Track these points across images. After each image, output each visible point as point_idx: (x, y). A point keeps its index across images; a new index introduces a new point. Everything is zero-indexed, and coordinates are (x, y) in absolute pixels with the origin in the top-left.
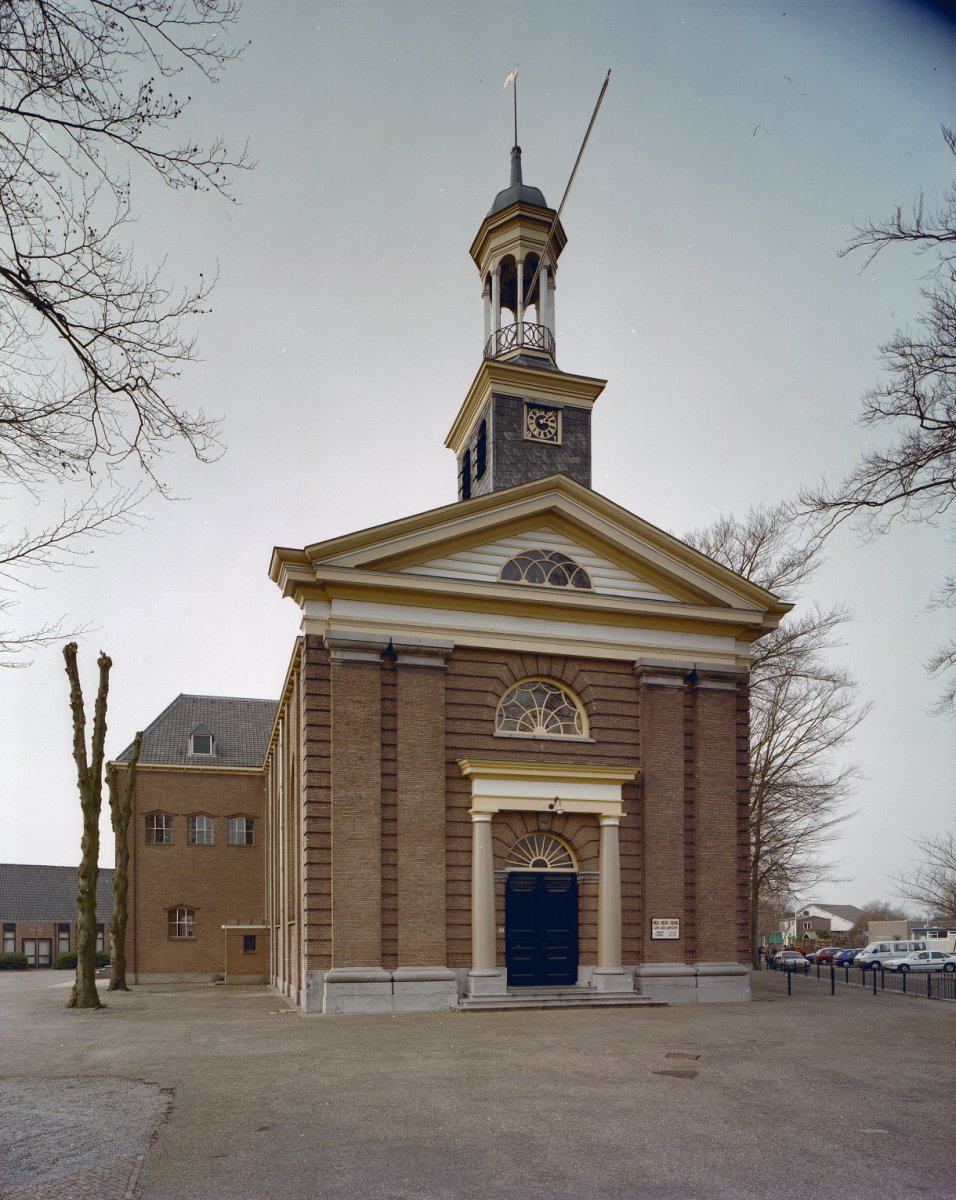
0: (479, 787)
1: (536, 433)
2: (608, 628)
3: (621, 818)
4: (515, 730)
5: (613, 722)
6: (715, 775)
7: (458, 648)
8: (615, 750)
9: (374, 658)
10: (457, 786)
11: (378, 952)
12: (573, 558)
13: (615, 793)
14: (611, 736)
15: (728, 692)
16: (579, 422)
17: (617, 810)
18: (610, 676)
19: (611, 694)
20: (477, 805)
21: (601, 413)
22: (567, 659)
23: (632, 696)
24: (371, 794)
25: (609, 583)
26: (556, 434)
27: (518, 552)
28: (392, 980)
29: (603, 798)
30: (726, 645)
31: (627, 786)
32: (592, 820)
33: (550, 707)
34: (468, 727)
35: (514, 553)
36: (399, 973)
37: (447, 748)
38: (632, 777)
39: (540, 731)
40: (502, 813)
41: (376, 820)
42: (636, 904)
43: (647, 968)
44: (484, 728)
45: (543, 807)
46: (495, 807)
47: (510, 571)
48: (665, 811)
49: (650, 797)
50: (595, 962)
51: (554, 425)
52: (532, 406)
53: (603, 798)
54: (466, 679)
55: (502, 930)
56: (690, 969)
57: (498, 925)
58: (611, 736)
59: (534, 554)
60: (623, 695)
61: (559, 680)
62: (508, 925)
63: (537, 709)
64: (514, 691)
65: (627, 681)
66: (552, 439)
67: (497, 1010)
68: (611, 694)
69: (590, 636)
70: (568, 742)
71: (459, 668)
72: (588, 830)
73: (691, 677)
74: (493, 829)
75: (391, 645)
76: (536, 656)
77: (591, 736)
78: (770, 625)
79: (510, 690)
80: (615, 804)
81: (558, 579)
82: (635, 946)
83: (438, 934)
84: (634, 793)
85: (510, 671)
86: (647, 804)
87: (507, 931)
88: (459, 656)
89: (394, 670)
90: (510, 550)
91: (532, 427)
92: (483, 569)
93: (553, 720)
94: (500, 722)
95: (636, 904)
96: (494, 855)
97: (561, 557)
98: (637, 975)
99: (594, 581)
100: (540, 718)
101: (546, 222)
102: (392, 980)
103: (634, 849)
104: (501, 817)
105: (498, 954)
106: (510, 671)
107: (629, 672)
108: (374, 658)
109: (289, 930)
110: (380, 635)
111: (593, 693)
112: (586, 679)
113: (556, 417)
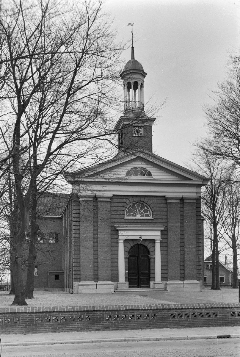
0: (120, 233)
2: (159, 187)
3: (161, 240)
4: (131, 216)
5: (159, 213)
6: (189, 227)
8: (160, 221)
9: (178, 201)
10: (115, 232)
11: (93, 277)
12: (147, 168)
13: (159, 233)
14: (158, 217)
15: (194, 203)
16: (149, 130)
17: (159, 238)
18: (158, 200)
19: (158, 205)
20: (120, 238)
21: (155, 127)
22: (145, 196)
23: (165, 205)
24: (91, 235)
25: (157, 175)
26: (142, 133)
27: (130, 168)
28: (97, 285)
29: (155, 234)
30: (194, 190)
31: (162, 231)
32: (153, 241)
33: (141, 209)
35: (129, 168)
38: (163, 229)
39: (138, 216)
40: (126, 239)
41: (92, 242)
42: (166, 264)
43: (169, 282)
44: (121, 216)
45: (138, 238)
46: (124, 238)
47: (128, 173)
48: (174, 237)
49: (170, 234)
50: (154, 280)
51: (141, 131)
53: (155, 234)
54: (117, 203)
55: (127, 271)
56: (182, 282)
58: (158, 217)
59: (136, 168)
60: (162, 205)
61: (143, 202)
62: (129, 270)
63: (137, 210)
64: (131, 205)
65: (163, 201)
68: (158, 205)
69: (136, 189)
70: (128, 219)
71: (115, 200)
72: (152, 243)
74: (124, 244)
75: (95, 196)
76: (136, 196)
77: (153, 218)
78: (205, 183)
79: (129, 205)
80: (159, 237)
82: (166, 276)
83: (109, 273)
84: (164, 233)
85: (129, 200)
86: (169, 236)
87: (128, 272)
88: (115, 197)
89: (97, 202)
90: (129, 167)
92: (121, 173)
93: (142, 213)
95: (166, 264)
96: (124, 251)
98: (166, 284)
99: (153, 174)
100: (138, 212)
102: (183, 284)
103: (165, 248)
104: (126, 241)
105: (126, 278)
106: (129, 200)
107: (164, 199)
108: (178, 201)
109: (70, 272)
110: (180, 195)
111: (155, 209)
112: (152, 201)
113: (142, 129)
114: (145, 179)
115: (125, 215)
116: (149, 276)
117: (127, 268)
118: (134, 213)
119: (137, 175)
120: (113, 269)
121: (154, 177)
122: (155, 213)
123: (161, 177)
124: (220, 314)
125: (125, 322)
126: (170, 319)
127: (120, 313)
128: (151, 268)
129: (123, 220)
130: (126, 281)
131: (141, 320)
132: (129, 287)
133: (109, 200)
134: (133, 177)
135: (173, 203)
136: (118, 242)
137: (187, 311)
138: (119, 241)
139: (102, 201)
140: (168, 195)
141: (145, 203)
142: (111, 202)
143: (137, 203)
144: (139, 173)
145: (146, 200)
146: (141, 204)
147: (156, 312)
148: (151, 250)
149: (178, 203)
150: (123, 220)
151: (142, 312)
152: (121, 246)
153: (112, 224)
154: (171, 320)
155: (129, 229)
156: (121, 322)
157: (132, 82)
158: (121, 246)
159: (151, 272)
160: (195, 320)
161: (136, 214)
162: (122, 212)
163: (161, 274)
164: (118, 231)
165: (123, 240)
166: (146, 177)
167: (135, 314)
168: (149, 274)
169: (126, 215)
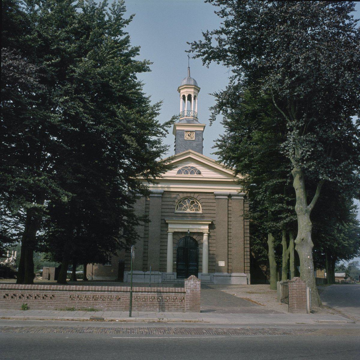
0: (169, 226)
1: (188, 138)
7: (165, 191)
13: (207, 227)
14: (207, 212)
20: (170, 230)
31: (210, 225)
34: (168, 210)
36: (146, 273)
37: (162, 216)
38: (210, 223)
39: (188, 211)
44: (172, 210)
45: (187, 231)
47: (179, 172)
50: (201, 272)
52: (187, 131)
55: (175, 262)
57: (174, 261)
58: (207, 212)
62: (177, 261)
65: (213, 197)
66: (192, 138)
67: (238, 276)
73: (230, 196)
81: (192, 173)
87: (177, 263)
91: (187, 136)
94: (177, 209)
96: (173, 243)
97: (192, 167)
99: (202, 173)
101: (197, 89)
102: (145, 274)
104: (175, 233)
110: (228, 192)
111: (204, 204)
112: (201, 197)
114: (195, 177)
115: (176, 209)
116: (198, 267)
117: (175, 259)
118: (185, 207)
119: (187, 173)
120: (161, 260)
121: (203, 175)
122: (205, 208)
123: (214, 175)
124: (123, 298)
125: (22, 301)
126: (69, 300)
127: (18, 292)
128: (200, 260)
129: (173, 214)
130: (173, 272)
131: (39, 300)
132: (177, 278)
133: (161, 195)
134: (183, 175)
135: (220, 199)
136: (167, 235)
137: (88, 293)
138: (168, 234)
139: (235, 199)
140: (216, 191)
141: (194, 198)
142: (162, 197)
143: (187, 198)
144: (183, 171)
145: (196, 195)
146: (191, 199)
147: (56, 293)
148: (199, 243)
149: (226, 199)
150: (173, 214)
151: (41, 293)
152: (170, 238)
153: (163, 218)
154: (70, 302)
155: (178, 222)
156: (18, 301)
157: (186, 96)
158: (170, 238)
159: (200, 263)
160: (96, 303)
161: (191, 209)
162: (173, 207)
163: (168, 249)
164: (167, 224)
165: (172, 232)
166: (195, 175)
167: (25, 294)
168: (197, 266)
169: (177, 209)
